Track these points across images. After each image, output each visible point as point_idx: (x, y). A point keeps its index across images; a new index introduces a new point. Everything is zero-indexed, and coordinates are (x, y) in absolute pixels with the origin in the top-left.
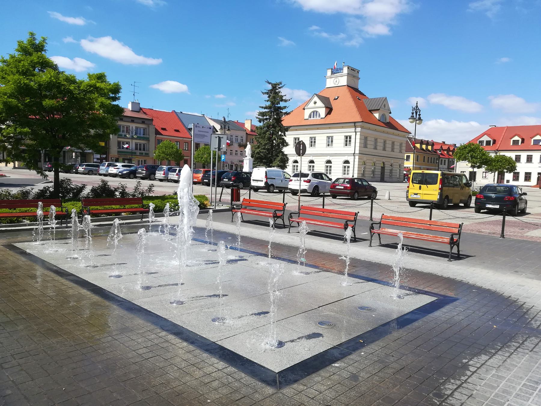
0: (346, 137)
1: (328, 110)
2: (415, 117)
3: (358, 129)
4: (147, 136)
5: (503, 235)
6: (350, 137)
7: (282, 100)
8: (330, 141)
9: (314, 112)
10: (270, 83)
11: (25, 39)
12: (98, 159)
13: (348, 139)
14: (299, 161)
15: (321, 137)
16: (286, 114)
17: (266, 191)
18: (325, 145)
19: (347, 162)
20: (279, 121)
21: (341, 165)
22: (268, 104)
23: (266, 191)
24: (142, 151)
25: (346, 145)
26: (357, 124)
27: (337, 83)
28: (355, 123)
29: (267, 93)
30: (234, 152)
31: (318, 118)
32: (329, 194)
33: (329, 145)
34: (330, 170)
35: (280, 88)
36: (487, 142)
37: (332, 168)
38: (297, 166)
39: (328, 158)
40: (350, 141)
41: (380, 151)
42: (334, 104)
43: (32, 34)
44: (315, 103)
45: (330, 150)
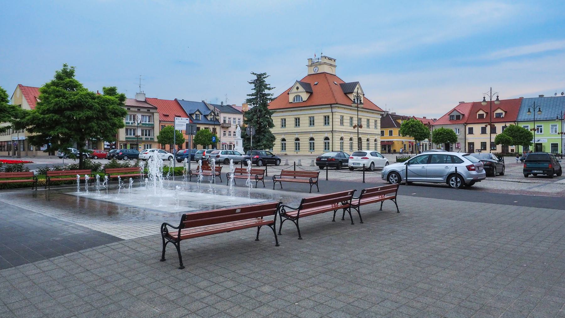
0: (325, 117)
2: (356, 102)
4: (152, 123)
5: (327, 179)
6: (328, 117)
7: (267, 88)
8: (297, 122)
9: (297, 96)
10: (255, 74)
11: (60, 69)
12: (108, 145)
14: (330, 137)
16: (271, 99)
19: (327, 139)
20: (265, 105)
22: (254, 92)
24: (147, 137)
26: (333, 106)
28: (331, 105)
29: (253, 83)
30: (232, 133)
31: (132, 136)
35: (264, 78)
36: (457, 116)
37: (315, 145)
38: (328, 143)
39: (297, 136)
42: (314, 89)
43: (65, 66)
44: (298, 88)
45: (312, 129)
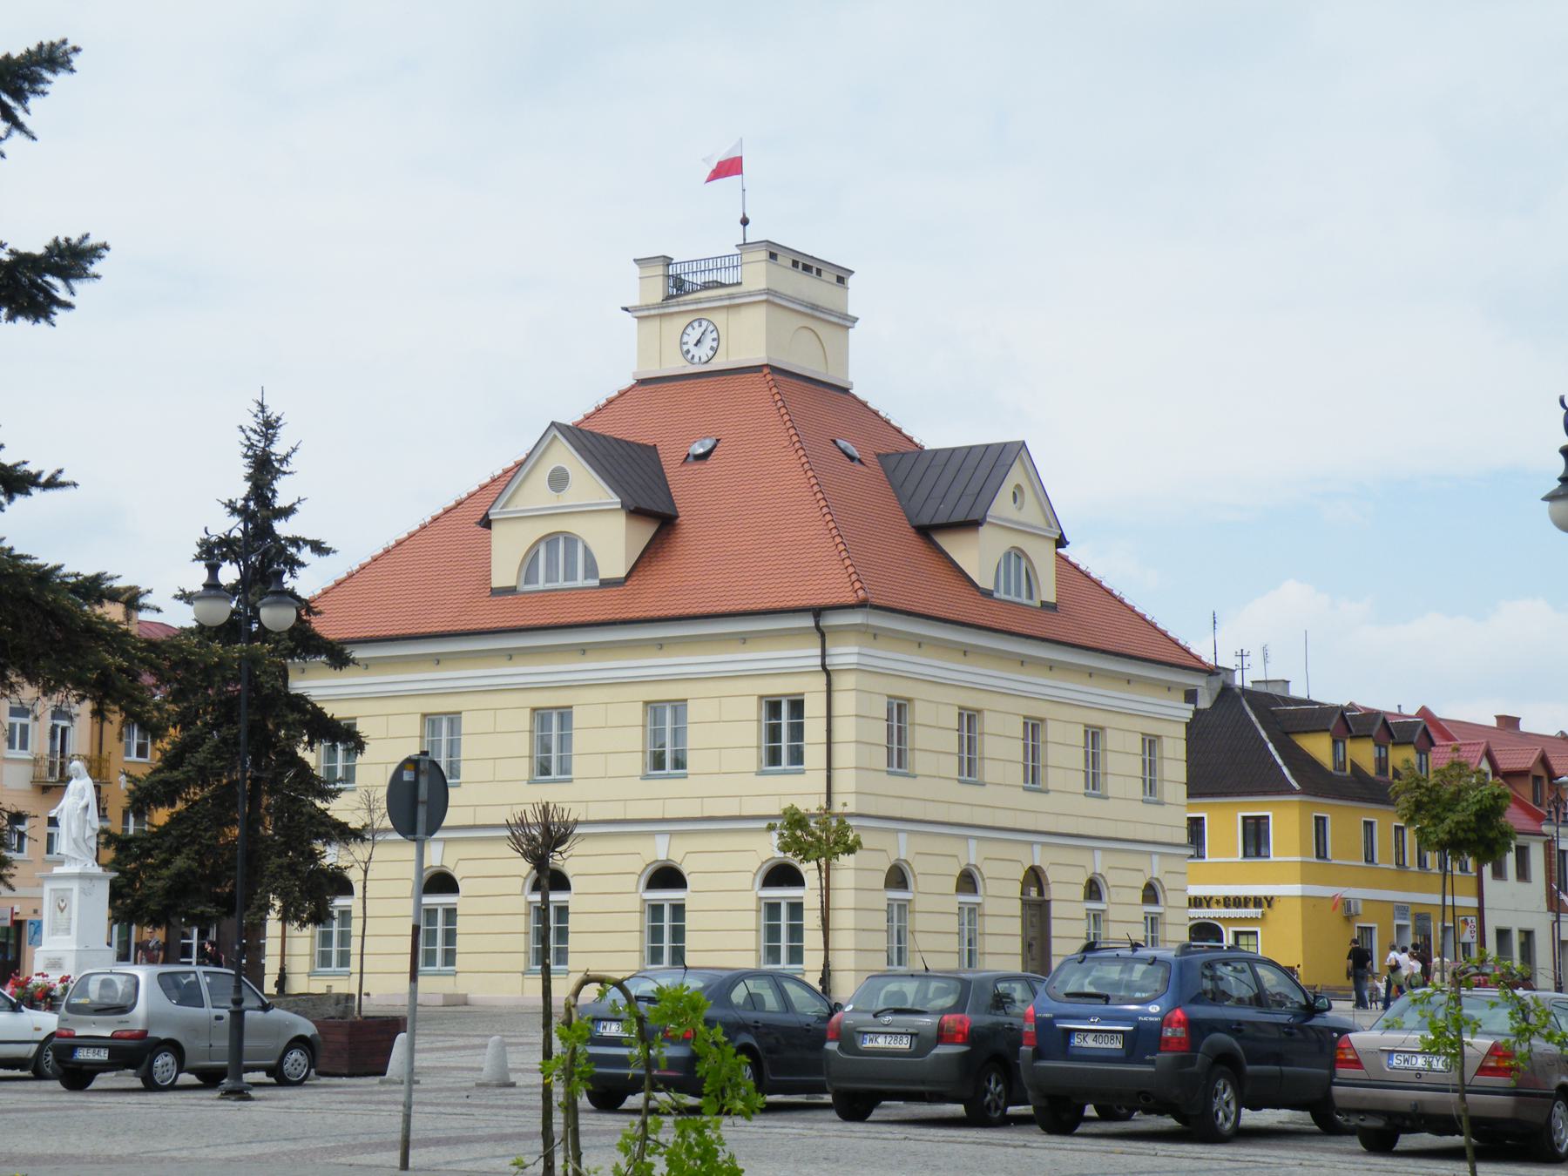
0: (774, 707)
1: (646, 532)
3: (844, 654)
6: (797, 706)
9: (550, 539)
13: (785, 720)
15: (606, 702)
17: (959, 1109)
18: (637, 763)
21: (635, 897)
23: (959, 1109)
25: (774, 757)
26: (831, 620)
27: (703, 352)
28: (818, 612)
31: (580, 582)
32: (828, 1099)
33: (545, 770)
34: (450, 936)
38: (796, 909)
39: (661, 850)
40: (797, 732)
41: (1064, 803)
42: (685, 489)
44: (559, 480)
